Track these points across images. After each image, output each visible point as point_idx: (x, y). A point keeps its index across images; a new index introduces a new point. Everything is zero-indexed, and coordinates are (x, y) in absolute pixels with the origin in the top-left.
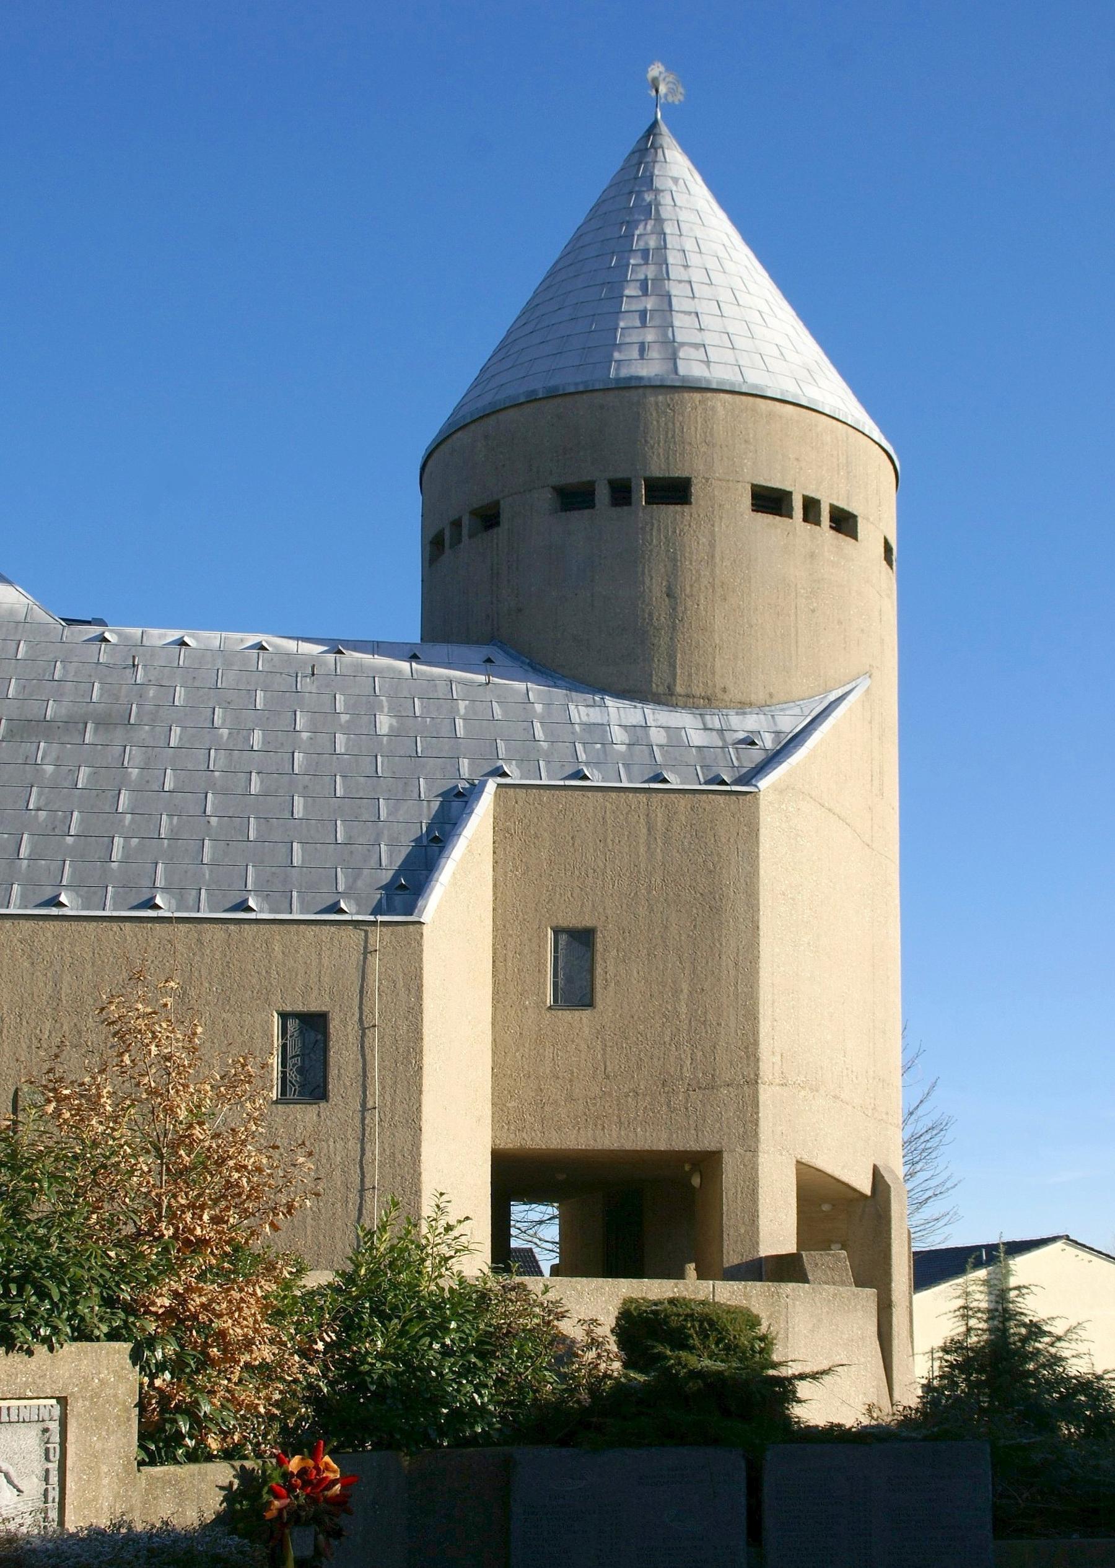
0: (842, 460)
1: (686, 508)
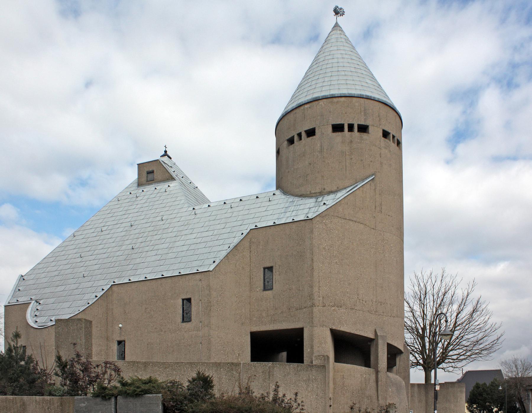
0: (363, 109)
1: (314, 137)
